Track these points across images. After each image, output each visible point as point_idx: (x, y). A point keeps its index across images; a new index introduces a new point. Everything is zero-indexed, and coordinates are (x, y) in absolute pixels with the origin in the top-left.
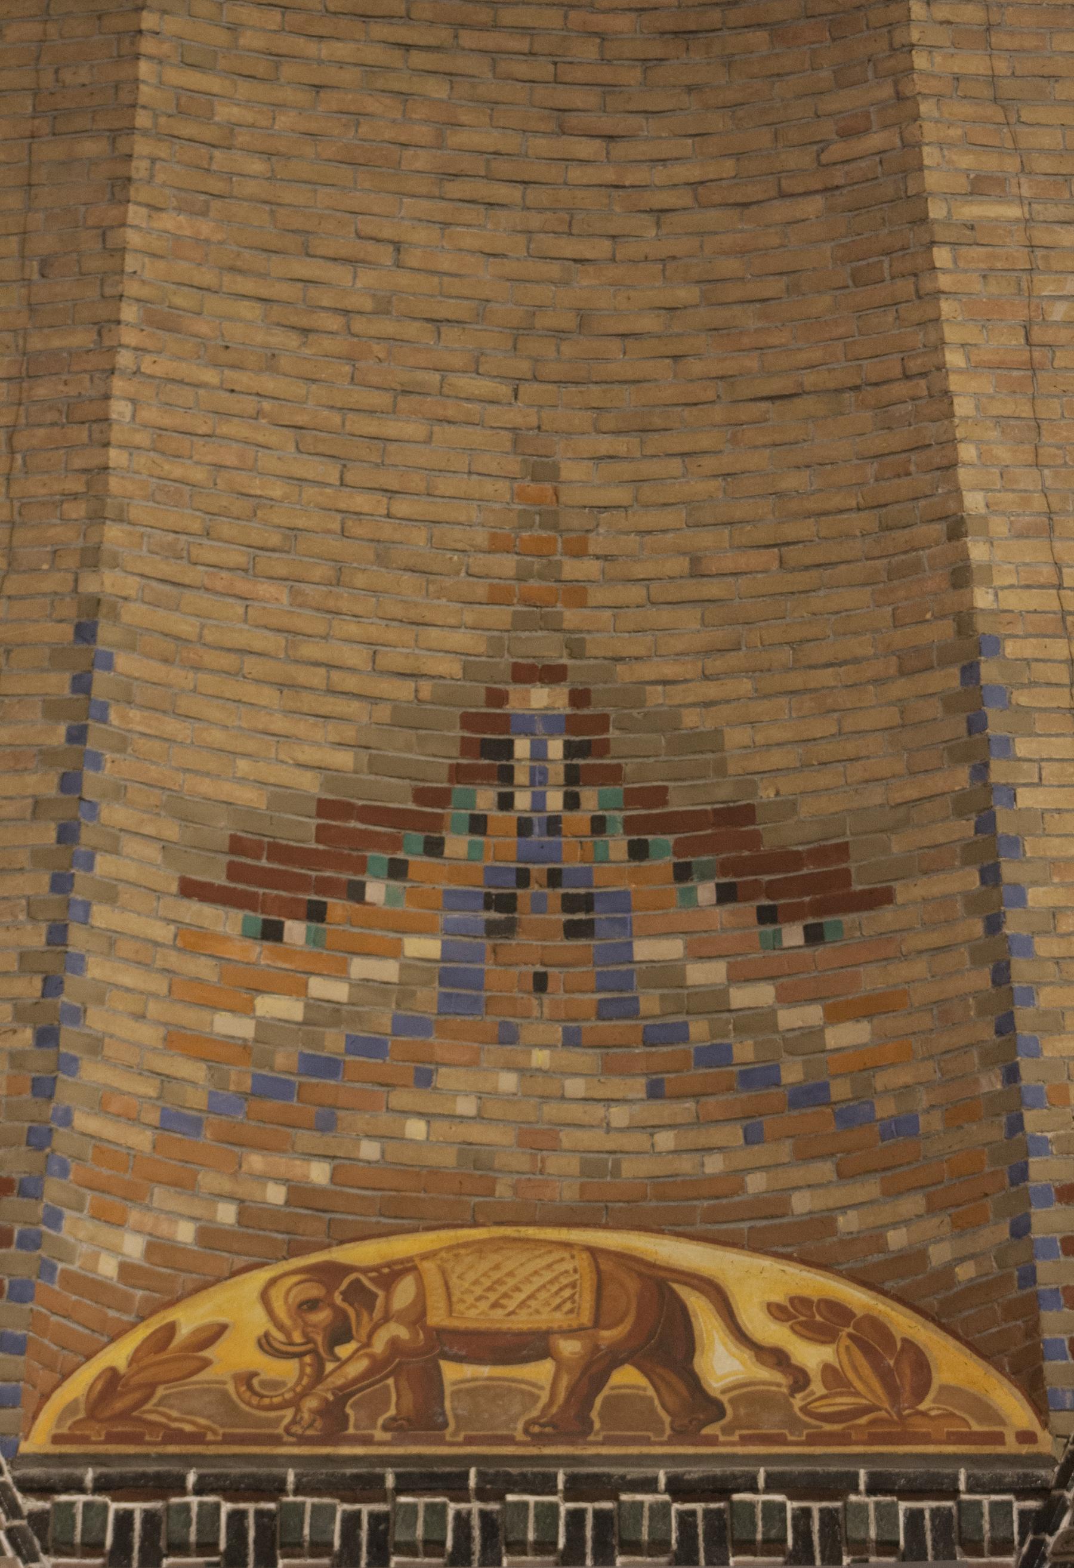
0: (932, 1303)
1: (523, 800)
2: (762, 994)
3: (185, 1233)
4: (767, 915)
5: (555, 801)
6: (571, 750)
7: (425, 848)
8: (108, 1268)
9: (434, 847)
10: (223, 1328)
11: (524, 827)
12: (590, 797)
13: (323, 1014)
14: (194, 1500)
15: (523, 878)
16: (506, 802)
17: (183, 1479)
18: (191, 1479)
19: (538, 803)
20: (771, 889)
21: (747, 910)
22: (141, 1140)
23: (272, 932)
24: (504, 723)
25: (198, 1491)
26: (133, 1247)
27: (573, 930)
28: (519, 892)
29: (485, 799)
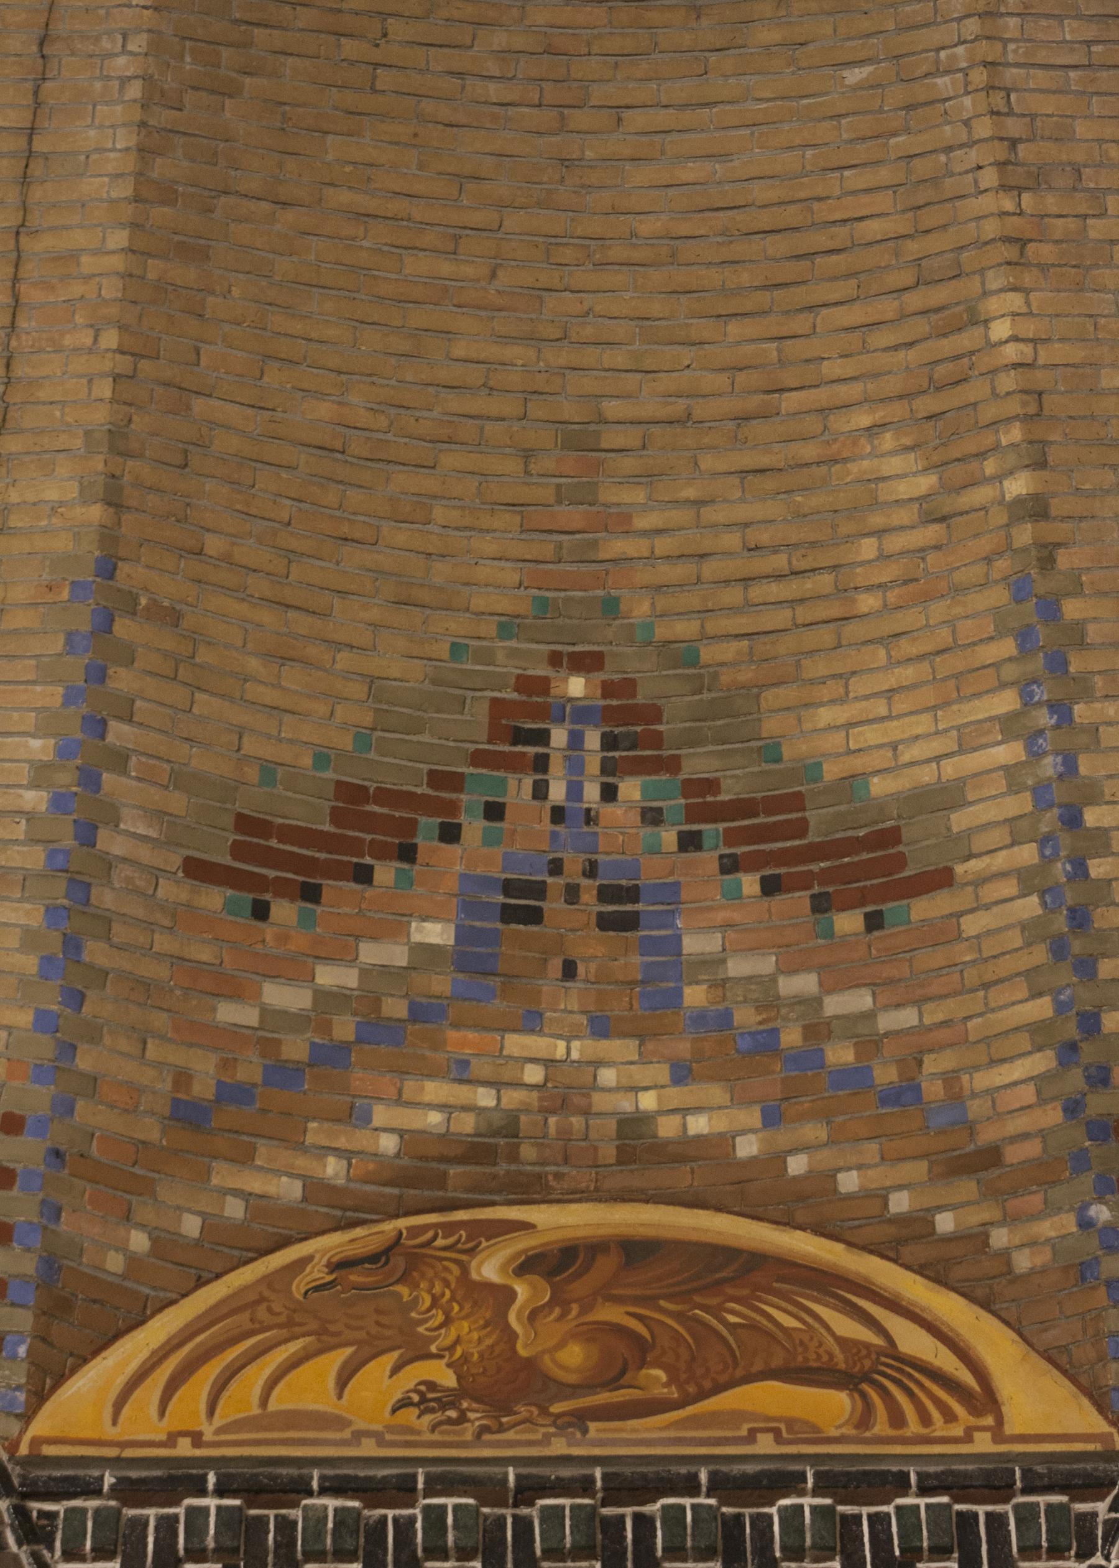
0: (979, 1293)
1: (557, 792)
2: (805, 983)
3: (191, 1226)
4: (821, 905)
5: (592, 792)
6: (609, 742)
7: (638, 919)
8: (115, 1263)
9: (450, 834)
10: (391, 1377)
11: (558, 814)
12: (631, 789)
13: (329, 1001)
14: (211, 1503)
15: (556, 867)
16: (540, 791)
17: (203, 1479)
18: (212, 1479)
19: (575, 791)
20: (825, 877)
21: (801, 900)
22: (151, 1131)
23: (261, 912)
24: (543, 712)
25: (220, 1492)
26: (139, 1241)
27: (605, 923)
28: (550, 880)
29: (518, 789)
